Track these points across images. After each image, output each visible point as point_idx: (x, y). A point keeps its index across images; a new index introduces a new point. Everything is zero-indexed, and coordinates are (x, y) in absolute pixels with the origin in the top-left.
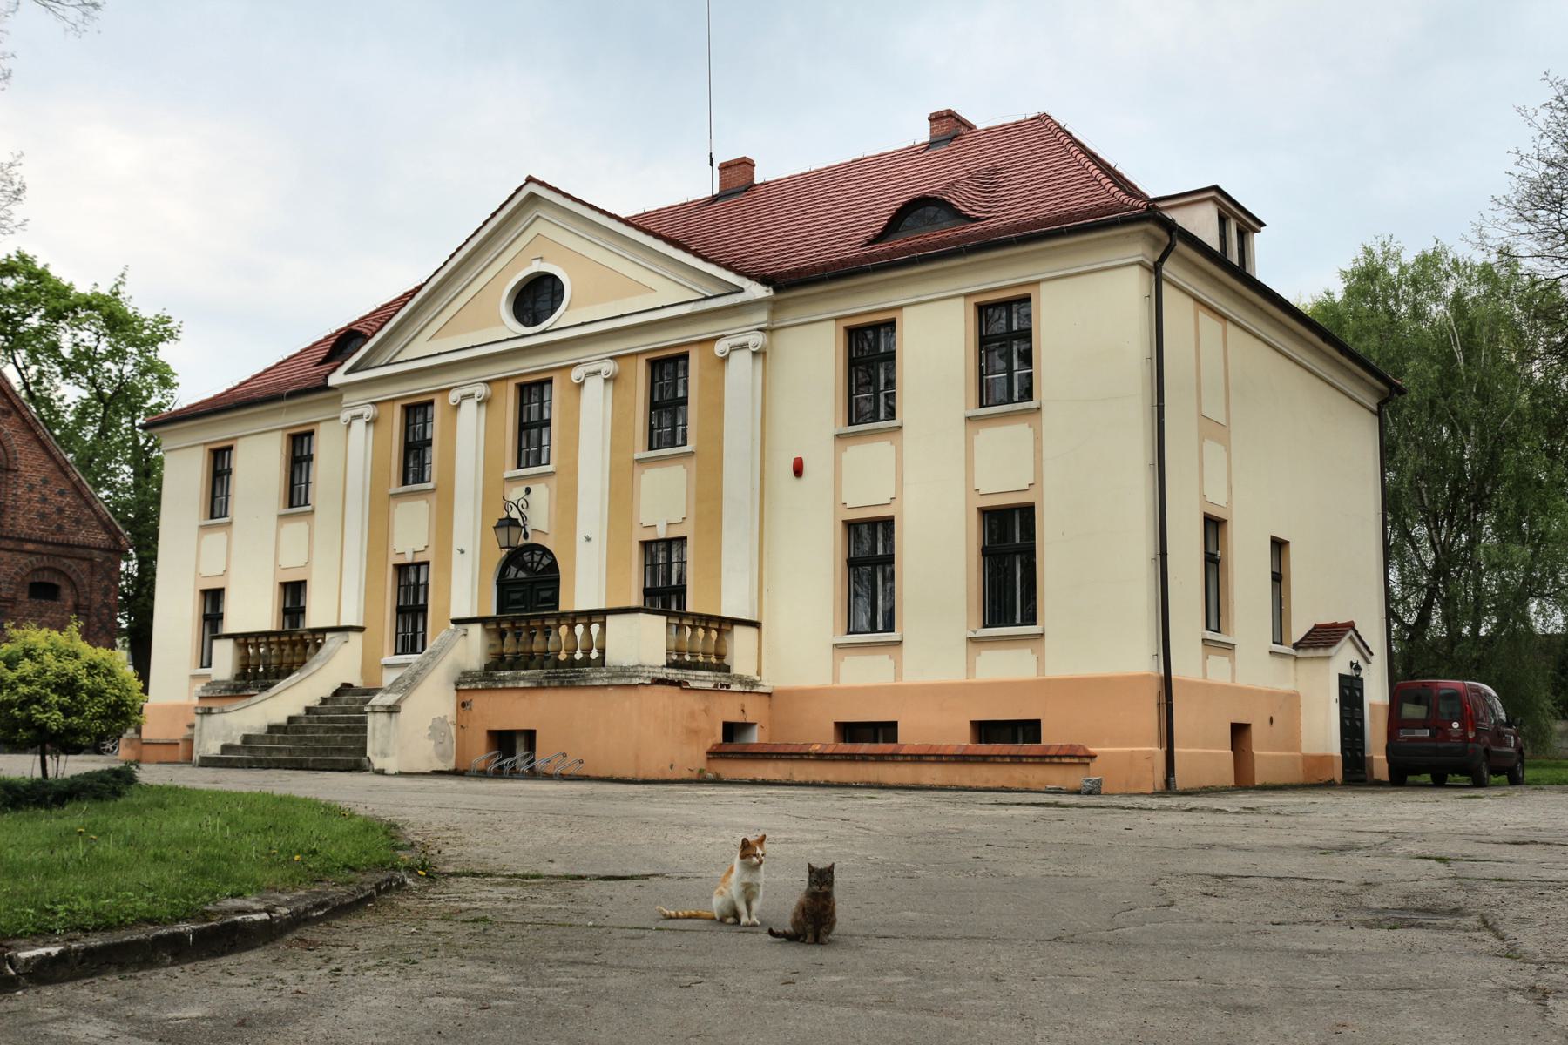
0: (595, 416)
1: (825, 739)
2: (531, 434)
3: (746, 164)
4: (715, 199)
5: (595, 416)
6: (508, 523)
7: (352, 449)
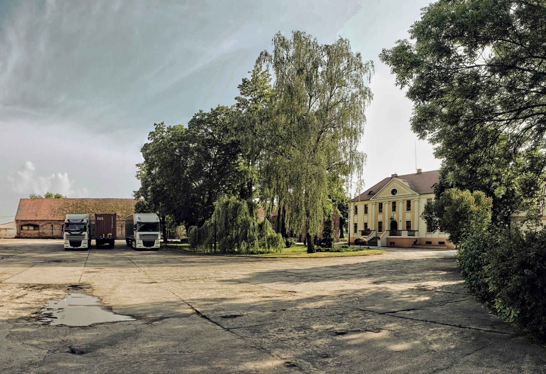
0: (401, 207)
1: (437, 243)
2: (394, 208)
3: (420, 170)
4: (417, 174)
5: (401, 207)
6: (391, 218)
7: (372, 208)
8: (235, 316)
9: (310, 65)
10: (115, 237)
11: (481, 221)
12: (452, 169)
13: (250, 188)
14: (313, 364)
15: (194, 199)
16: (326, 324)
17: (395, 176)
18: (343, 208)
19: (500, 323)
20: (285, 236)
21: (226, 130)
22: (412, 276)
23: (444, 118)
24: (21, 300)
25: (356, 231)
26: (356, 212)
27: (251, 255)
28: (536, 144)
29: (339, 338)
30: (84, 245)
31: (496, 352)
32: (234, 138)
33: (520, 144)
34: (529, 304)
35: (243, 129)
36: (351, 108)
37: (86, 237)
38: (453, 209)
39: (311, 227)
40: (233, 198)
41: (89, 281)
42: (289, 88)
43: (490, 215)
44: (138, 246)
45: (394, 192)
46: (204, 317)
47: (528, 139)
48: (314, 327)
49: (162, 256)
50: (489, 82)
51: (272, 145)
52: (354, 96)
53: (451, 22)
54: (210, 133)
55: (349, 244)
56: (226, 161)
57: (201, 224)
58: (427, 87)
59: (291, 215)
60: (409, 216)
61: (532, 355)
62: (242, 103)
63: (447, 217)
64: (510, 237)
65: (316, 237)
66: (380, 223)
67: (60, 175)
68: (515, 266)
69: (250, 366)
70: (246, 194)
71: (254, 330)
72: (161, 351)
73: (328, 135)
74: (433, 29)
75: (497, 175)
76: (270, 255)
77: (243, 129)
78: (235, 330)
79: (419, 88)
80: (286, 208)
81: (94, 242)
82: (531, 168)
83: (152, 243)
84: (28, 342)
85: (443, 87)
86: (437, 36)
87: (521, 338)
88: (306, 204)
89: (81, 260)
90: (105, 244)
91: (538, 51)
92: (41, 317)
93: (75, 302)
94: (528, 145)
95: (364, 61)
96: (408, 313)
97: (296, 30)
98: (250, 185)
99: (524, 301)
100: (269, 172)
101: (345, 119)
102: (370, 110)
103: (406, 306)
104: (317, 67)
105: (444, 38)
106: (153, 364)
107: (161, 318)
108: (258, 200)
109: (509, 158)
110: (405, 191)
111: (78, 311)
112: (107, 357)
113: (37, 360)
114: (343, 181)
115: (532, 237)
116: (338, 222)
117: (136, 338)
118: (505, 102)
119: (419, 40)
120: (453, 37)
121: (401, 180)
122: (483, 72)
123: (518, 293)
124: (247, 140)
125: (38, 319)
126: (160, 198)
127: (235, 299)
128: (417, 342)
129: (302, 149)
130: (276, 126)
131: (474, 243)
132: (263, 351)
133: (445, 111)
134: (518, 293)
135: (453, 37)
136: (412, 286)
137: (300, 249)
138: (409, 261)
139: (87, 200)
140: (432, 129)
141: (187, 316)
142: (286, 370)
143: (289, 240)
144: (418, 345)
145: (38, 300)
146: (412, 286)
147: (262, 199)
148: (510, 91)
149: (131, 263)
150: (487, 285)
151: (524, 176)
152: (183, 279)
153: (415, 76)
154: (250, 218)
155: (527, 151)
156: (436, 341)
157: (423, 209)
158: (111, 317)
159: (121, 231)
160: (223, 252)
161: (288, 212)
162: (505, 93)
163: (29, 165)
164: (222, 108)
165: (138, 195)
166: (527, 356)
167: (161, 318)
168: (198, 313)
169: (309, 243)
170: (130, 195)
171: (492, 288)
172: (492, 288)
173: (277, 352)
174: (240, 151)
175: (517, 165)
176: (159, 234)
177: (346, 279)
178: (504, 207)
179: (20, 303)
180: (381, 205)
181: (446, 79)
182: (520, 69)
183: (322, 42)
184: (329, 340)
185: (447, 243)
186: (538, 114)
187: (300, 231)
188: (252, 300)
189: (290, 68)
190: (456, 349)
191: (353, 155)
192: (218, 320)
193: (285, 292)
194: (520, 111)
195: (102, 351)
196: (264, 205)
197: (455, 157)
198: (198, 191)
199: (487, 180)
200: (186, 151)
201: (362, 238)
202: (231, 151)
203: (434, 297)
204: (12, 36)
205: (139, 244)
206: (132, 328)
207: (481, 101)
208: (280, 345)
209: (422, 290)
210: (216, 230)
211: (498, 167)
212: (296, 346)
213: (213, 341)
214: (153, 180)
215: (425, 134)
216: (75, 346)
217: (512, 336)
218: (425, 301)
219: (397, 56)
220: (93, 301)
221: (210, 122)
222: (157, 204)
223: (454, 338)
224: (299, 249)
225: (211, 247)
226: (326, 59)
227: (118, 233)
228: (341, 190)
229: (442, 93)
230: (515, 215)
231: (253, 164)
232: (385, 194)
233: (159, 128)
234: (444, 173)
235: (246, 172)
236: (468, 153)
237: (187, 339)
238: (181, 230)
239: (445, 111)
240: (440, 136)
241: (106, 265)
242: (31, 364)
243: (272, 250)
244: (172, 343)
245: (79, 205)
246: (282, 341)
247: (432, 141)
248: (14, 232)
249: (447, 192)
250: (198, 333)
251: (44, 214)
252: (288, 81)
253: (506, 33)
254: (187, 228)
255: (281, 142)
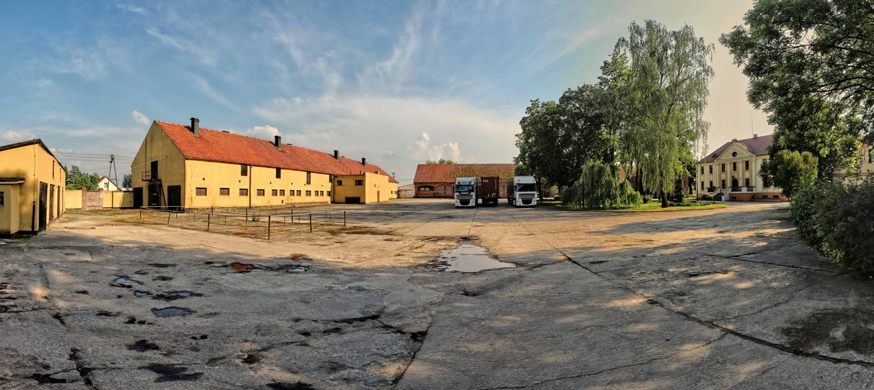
0: (741, 167)
2: (735, 168)
5: (741, 167)
7: (716, 168)
8: (601, 262)
9: (660, 49)
10: (498, 197)
11: (809, 178)
12: (783, 134)
13: (612, 153)
14: (672, 301)
15: (565, 164)
16: (681, 267)
17: (735, 141)
18: (691, 169)
19: (827, 263)
20: (642, 193)
21: (591, 105)
22: (751, 225)
23: (774, 90)
24: (419, 250)
25: (703, 188)
26: (703, 172)
27: (614, 210)
28: (854, 111)
29: (693, 279)
30: (472, 203)
31: (825, 288)
32: (598, 111)
33: (840, 111)
34: (853, 246)
35: (605, 103)
36: (696, 84)
37: (474, 197)
38: (785, 168)
39: (665, 185)
40: (598, 162)
41: (477, 234)
42: (644, 68)
43: (816, 172)
44: (518, 204)
45: (734, 154)
46: (575, 262)
47: (847, 106)
48: (671, 270)
49: (538, 212)
50: (812, 59)
51: (630, 116)
52: (698, 74)
53: (779, 10)
54: (578, 108)
55: (698, 199)
56: (591, 131)
57: (571, 185)
58: (760, 65)
59: (648, 175)
60: (747, 175)
61: (856, 290)
62: (604, 82)
63: (780, 174)
64: (835, 190)
65: (669, 194)
66: (724, 181)
67: (451, 144)
68: (840, 214)
69: (619, 303)
70: (608, 158)
71: (620, 273)
72: (542, 292)
73: (677, 108)
74: (764, 16)
75: (821, 137)
76: (630, 210)
77: (605, 103)
78: (602, 274)
79: (753, 65)
80: (643, 170)
81: (480, 201)
82: (850, 131)
83: (530, 201)
84: (427, 285)
85: (774, 64)
86: (767, 22)
87: (846, 276)
88: (660, 166)
89: (469, 216)
90: (490, 202)
91: (853, 32)
92: (437, 265)
93: (466, 251)
94: (847, 112)
95: (706, 44)
96: (749, 256)
97: (648, 20)
98: (612, 151)
99: (848, 243)
100: (627, 139)
101: (691, 92)
102: (711, 84)
103: (747, 251)
104: (667, 50)
105: (774, 23)
106: (537, 303)
107: (541, 265)
108: (619, 163)
109: (832, 123)
110: (744, 153)
111: (468, 260)
112: (497, 299)
113: (437, 301)
114: (691, 146)
115: (853, 190)
116: (687, 180)
117: (521, 282)
118: (827, 76)
119: (752, 25)
120: (781, 22)
121: (740, 144)
122: (807, 51)
123: (843, 237)
124: (609, 112)
125: (435, 266)
126: (536, 163)
127: (601, 247)
128: (758, 281)
129: (656, 119)
130: (633, 100)
131: (803, 196)
132: (627, 291)
133: (776, 84)
134: (843, 237)
135: (781, 22)
136: (752, 233)
137: (655, 204)
138: (748, 213)
139: (474, 165)
140: (765, 100)
141: (560, 262)
142: (649, 306)
143: (646, 197)
144: (759, 283)
145: (434, 250)
146: (752, 233)
147: (622, 163)
148: (830, 67)
149: (513, 218)
150: (815, 231)
151: (844, 138)
152: (557, 231)
153: (750, 56)
154: (612, 179)
155: (847, 117)
156: (775, 280)
157: (759, 168)
158: (497, 264)
159: (503, 191)
160: (590, 208)
161: (644, 173)
162: (827, 68)
163: (425, 135)
164: (588, 86)
165: (517, 160)
166: (852, 291)
167: (541, 265)
168: (569, 259)
169: (663, 199)
170: (510, 161)
171: (819, 234)
172: (819, 234)
173: (641, 291)
174: (603, 122)
175: (838, 129)
176: (536, 193)
177: (695, 229)
178: (827, 164)
179: (418, 253)
180: (723, 165)
181: (776, 58)
182: (838, 48)
183: (670, 29)
184: (684, 281)
185: (780, 197)
186: (855, 85)
187: (654, 189)
188: (616, 248)
189: (644, 51)
190: (790, 286)
191: (698, 123)
192: (587, 265)
193: (643, 241)
194: (839, 82)
195: (491, 293)
196: (624, 168)
197: (786, 124)
198: (568, 157)
199: (814, 142)
200: (558, 123)
201: (708, 194)
202: (596, 122)
203: (770, 243)
204: (410, 28)
205: (519, 202)
206: (516, 273)
207: (806, 75)
208: (643, 285)
209: (760, 237)
210: (584, 189)
211: (822, 131)
212: (656, 286)
213: (582, 282)
214: (530, 148)
215: (759, 105)
216: (468, 289)
217: (839, 275)
218: (763, 246)
219: (734, 40)
220: (481, 250)
221: (577, 99)
222: (533, 168)
223: (789, 276)
224: (655, 204)
225: (580, 204)
226: (674, 43)
227: (501, 193)
228: (689, 153)
229: (773, 69)
230: (836, 172)
231: (614, 133)
232: (727, 157)
233: (535, 104)
234: (776, 137)
235: (608, 140)
236: (796, 120)
237: (564, 283)
238: (555, 189)
239: (776, 84)
240: (773, 106)
241: (491, 220)
242: (432, 304)
243: (631, 205)
244: (551, 286)
245: (467, 170)
246: (644, 282)
247: (766, 110)
248: (413, 193)
249: (779, 153)
250: (570, 277)
251: (438, 177)
252: (642, 62)
253: (825, 18)
254: (559, 188)
255: (637, 114)
